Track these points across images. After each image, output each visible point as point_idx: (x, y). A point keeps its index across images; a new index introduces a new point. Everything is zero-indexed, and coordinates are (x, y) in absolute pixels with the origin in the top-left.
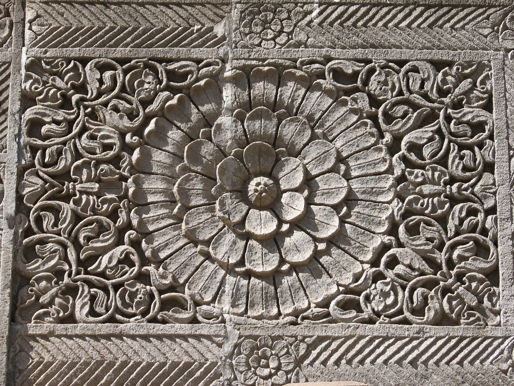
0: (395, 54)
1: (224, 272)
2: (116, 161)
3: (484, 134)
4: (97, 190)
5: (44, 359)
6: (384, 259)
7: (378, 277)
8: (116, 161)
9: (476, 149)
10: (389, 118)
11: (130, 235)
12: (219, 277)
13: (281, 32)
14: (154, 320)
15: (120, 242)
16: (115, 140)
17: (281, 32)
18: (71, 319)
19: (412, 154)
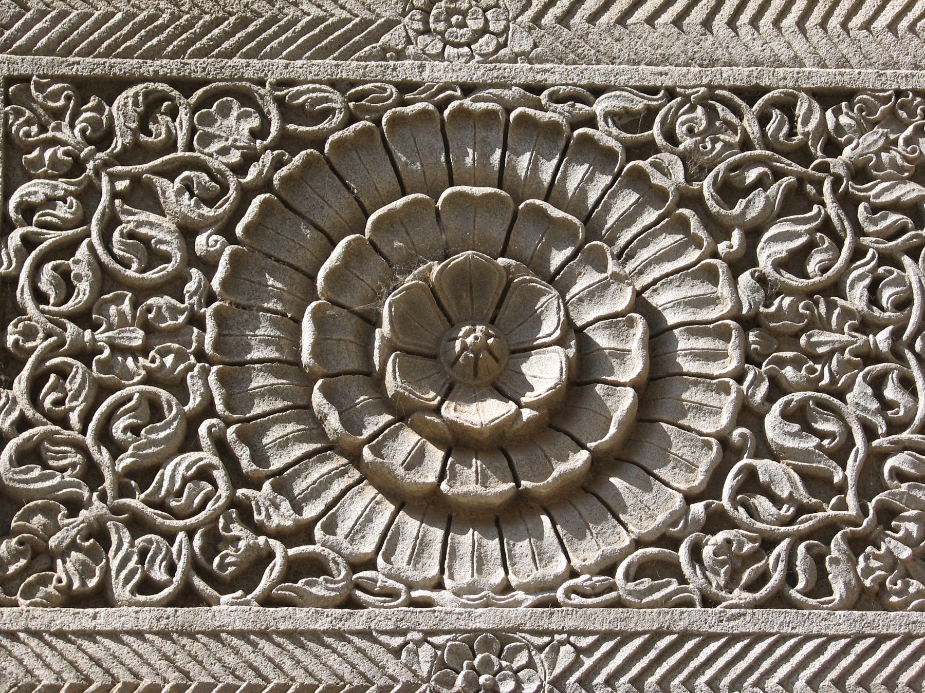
0: (742, 75)
1: (392, 508)
2: (174, 285)
3: (170, 265)
4: (139, 342)
5: (40, 682)
6: (729, 483)
7: (717, 521)
8: (174, 285)
9: (906, 260)
10: (730, 191)
11: (210, 428)
12: (380, 522)
13: (485, 30)
14: (267, 601)
15: (190, 443)
16: (173, 247)
17: (485, 30)
18: (101, 597)
19: (104, 450)
